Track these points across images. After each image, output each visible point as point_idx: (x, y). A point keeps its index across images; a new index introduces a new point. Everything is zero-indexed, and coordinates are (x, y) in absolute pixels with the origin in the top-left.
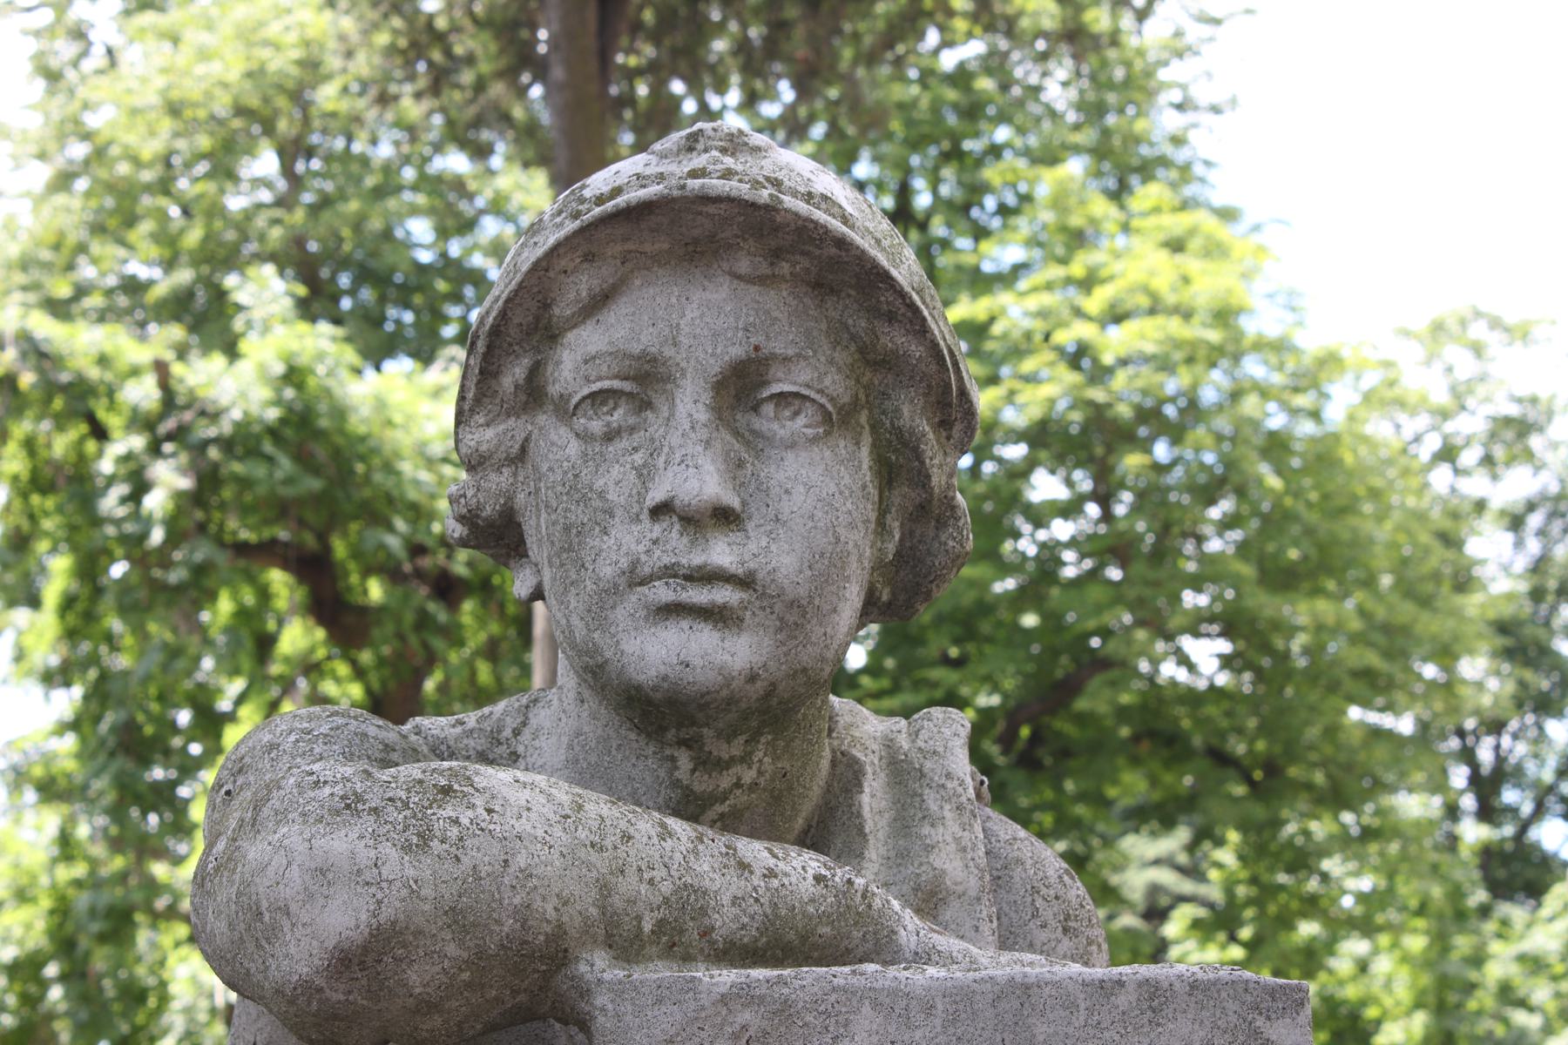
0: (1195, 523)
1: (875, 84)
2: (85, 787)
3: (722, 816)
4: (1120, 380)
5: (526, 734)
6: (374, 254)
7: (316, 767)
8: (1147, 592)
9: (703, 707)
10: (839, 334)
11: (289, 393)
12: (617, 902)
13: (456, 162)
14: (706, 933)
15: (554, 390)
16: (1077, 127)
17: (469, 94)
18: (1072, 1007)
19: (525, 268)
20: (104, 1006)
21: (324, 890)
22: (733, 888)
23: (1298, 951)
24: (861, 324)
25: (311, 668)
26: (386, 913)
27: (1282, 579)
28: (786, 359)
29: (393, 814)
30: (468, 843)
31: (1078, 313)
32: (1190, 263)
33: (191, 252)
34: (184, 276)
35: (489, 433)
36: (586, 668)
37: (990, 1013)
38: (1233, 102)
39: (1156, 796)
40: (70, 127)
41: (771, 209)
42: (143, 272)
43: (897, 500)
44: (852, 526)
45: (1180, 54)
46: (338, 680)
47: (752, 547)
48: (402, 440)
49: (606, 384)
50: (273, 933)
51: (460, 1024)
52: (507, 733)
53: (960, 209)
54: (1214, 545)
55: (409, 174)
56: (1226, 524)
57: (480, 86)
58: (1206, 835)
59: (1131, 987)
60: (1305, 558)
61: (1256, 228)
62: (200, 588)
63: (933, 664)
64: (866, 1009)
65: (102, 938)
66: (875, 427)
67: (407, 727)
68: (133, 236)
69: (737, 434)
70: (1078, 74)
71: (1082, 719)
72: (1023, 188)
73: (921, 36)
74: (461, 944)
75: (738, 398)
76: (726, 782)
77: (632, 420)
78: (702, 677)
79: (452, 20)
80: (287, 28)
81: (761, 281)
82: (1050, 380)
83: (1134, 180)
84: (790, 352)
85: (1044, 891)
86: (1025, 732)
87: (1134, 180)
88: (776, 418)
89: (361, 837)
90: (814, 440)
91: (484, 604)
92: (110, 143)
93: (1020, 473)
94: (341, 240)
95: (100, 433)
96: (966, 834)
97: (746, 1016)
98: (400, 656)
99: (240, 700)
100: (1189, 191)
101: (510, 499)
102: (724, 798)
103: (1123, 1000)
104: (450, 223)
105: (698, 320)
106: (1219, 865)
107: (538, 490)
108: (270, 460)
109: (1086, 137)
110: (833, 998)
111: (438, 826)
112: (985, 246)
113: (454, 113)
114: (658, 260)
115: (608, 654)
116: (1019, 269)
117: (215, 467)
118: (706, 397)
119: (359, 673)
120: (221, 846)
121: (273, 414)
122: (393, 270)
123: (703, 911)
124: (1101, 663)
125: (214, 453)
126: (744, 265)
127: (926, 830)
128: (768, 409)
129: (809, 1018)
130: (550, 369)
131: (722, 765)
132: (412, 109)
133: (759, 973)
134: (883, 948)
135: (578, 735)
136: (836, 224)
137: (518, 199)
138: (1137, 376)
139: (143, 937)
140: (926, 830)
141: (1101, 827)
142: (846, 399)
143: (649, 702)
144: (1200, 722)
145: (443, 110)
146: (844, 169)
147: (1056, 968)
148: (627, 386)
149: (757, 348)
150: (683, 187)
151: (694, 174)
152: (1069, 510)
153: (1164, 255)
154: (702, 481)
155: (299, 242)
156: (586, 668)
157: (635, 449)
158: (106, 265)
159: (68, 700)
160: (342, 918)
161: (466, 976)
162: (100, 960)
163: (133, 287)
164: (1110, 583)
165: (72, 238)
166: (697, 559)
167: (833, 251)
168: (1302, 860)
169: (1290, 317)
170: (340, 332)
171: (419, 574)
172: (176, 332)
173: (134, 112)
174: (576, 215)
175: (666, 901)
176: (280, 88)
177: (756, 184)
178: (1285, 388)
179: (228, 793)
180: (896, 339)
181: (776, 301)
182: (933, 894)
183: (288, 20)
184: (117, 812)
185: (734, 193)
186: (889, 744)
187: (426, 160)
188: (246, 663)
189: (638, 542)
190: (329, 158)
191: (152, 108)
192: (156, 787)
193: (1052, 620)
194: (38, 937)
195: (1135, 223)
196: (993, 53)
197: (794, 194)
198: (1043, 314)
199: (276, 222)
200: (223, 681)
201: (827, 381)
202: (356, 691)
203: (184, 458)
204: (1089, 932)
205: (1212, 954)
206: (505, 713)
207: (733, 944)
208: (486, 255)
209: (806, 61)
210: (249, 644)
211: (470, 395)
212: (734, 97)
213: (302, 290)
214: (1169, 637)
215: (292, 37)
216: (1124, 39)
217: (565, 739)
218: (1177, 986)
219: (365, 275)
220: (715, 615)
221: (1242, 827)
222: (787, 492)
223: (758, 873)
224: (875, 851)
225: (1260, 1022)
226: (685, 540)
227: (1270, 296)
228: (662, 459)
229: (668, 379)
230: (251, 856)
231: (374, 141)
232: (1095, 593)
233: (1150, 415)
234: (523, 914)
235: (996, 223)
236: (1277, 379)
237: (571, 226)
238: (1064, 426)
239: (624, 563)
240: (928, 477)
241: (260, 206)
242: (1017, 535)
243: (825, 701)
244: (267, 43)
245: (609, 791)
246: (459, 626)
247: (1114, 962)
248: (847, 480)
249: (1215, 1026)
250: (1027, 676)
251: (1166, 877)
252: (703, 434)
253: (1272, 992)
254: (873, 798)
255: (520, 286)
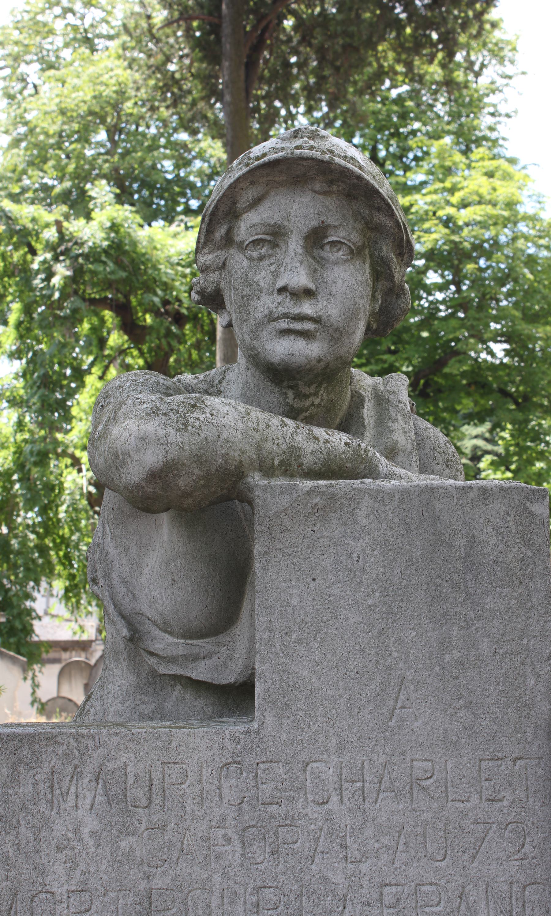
0: (495, 294)
1: (363, 104)
2: (27, 401)
3: (306, 418)
4: (466, 232)
5: (224, 383)
6: (147, 176)
7: (140, 396)
8: (475, 323)
9: (299, 372)
10: (357, 216)
11: (113, 235)
12: (264, 452)
13: (183, 136)
14: (300, 465)
15: (237, 239)
16: (449, 123)
17: (189, 106)
18: (451, 497)
19: (225, 187)
20: (37, 492)
21: (145, 447)
22: (311, 447)
23: (534, 474)
24: (366, 212)
25: (122, 352)
26: (170, 457)
27: (533, 318)
28: (335, 227)
29: (172, 415)
30: (203, 428)
31: (448, 203)
32: (496, 182)
33: (70, 174)
34: (67, 184)
35: (210, 257)
36: (250, 356)
37: (417, 499)
38: (516, 112)
39: (477, 409)
40: (18, 120)
41: (330, 163)
42: (50, 182)
43: (380, 287)
44: (361, 297)
45: (493, 92)
46: (133, 357)
47: (320, 306)
48: (160, 255)
49: (259, 237)
50: (123, 464)
51: (199, 502)
52: (216, 382)
53: (399, 157)
54: (504, 303)
55: (163, 141)
56: (509, 294)
57: (194, 103)
58: (497, 426)
59: (475, 489)
60: (542, 308)
61: (524, 168)
62: (75, 318)
63: (385, 353)
64: (366, 497)
65: (36, 464)
66: (371, 256)
67: (175, 379)
68: (46, 167)
69: (314, 258)
70: (450, 100)
71: (446, 376)
72: (425, 149)
73: (383, 83)
74: (200, 469)
75: (314, 242)
76: (307, 403)
77: (270, 252)
78: (299, 360)
79: (182, 74)
80: (111, 77)
81: (325, 193)
82: (435, 232)
83: (473, 146)
84: (337, 224)
85: (438, 449)
86: (422, 382)
87: (473, 146)
88: (331, 251)
89: (159, 425)
90: (346, 261)
91: (195, 326)
92: (36, 127)
93: (423, 272)
94: (134, 169)
95: (33, 252)
96: (407, 425)
97: (317, 500)
98: (159, 347)
99: (92, 365)
100: (496, 151)
101: (218, 284)
102: (307, 410)
103: (472, 495)
104: (181, 162)
105: (298, 210)
106: (503, 438)
107: (230, 281)
108: (105, 263)
109: (453, 127)
110: (353, 493)
111: (191, 421)
112: (408, 174)
113: (182, 115)
114: (281, 184)
115: (260, 350)
116: (423, 184)
117: (82, 265)
118: (301, 243)
119: (142, 354)
120: (100, 428)
121: (105, 244)
122: (156, 182)
123: (299, 457)
124: (455, 353)
125: (80, 260)
126: (318, 186)
127: (390, 424)
128: (327, 248)
129: (343, 501)
130: (236, 230)
131: (306, 396)
132: (164, 112)
133: (322, 482)
134: (372, 472)
135: (246, 383)
136: (356, 169)
137: (210, 151)
138: (473, 230)
139: (52, 463)
140: (390, 424)
141: (453, 422)
142: (360, 244)
143: (276, 370)
144: (496, 378)
145: (177, 113)
146: (350, 141)
147: (444, 481)
148: (268, 237)
149: (323, 222)
150: (293, 153)
151: (297, 148)
152: (442, 288)
153: (485, 178)
154: (300, 278)
155: (116, 170)
156: (250, 356)
157: (271, 264)
158: (34, 179)
159: (18, 365)
160: (152, 458)
161: (202, 482)
162: (35, 473)
163: (46, 188)
164: (460, 318)
165: (20, 168)
166: (297, 311)
167: (355, 181)
168: (536, 437)
169: (538, 206)
170: (134, 209)
171: (167, 312)
172: (65, 208)
173: (46, 113)
174: (247, 165)
175: (284, 452)
176: (108, 103)
177: (323, 152)
178: (535, 236)
179: (102, 406)
180: (381, 218)
181: (330, 202)
182: (393, 450)
183: (111, 74)
184: (40, 412)
185: (314, 156)
186: (375, 388)
187: (171, 135)
188: (95, 350)
189: (273, 303)
190: (128, 134)
191: (54, 111)
192: (57, 401)
193: (434, 334)
194: (9, 464)
195: (473, 164)
196: (413, 91)
197: (339, 157)
198: (432, 203)
199: (106, 161)
200: (84, 357)
201: (352, 236)
202: (141, 362)
203: (68, 262)
204: (457, 467)
205: (499, 475)
206: (215, 374)
207: (311, 470)
208: (195, 177)
209: (333, 93)
210: (95, 342)
211: (202, 241)
212: (302, 109)
213: (118, 191)
214: (484, 342)
215: (113, 81)
216: (470, 85)
217: (241, 385)
218: (494, 488)
219: (144, 184)
220: (305, 334)
221: (513, 423)
222: (335, 283)
223: (322, 441)
224: (369, 433)
225: (528, 504)
226: (292, 303)
227: (529, 196)
228: (283, 269)
229: (285, 234)
230: (114, 432)
231: (148, 127)
232: (453, 323)
233: (478, 247)
234: (226, 457)
235: (413, 163)
236: (532, 232)
237: (245, 170)
238: (441, 252)
239: (266, 312)
240: (393, 277)
241: (100, 154)
242: (421, 298)
243: (349, 370)
244: (102, 83)
245: (259, 406)
246: (184, 335)
247: (467, 480)
248: (360, 278)
249: (510, 505)
250: (423, 358)
251: (480, 443)
252: (300, 258)
253: (533, 492)
254: (368, 411)
255: (224, 195)
